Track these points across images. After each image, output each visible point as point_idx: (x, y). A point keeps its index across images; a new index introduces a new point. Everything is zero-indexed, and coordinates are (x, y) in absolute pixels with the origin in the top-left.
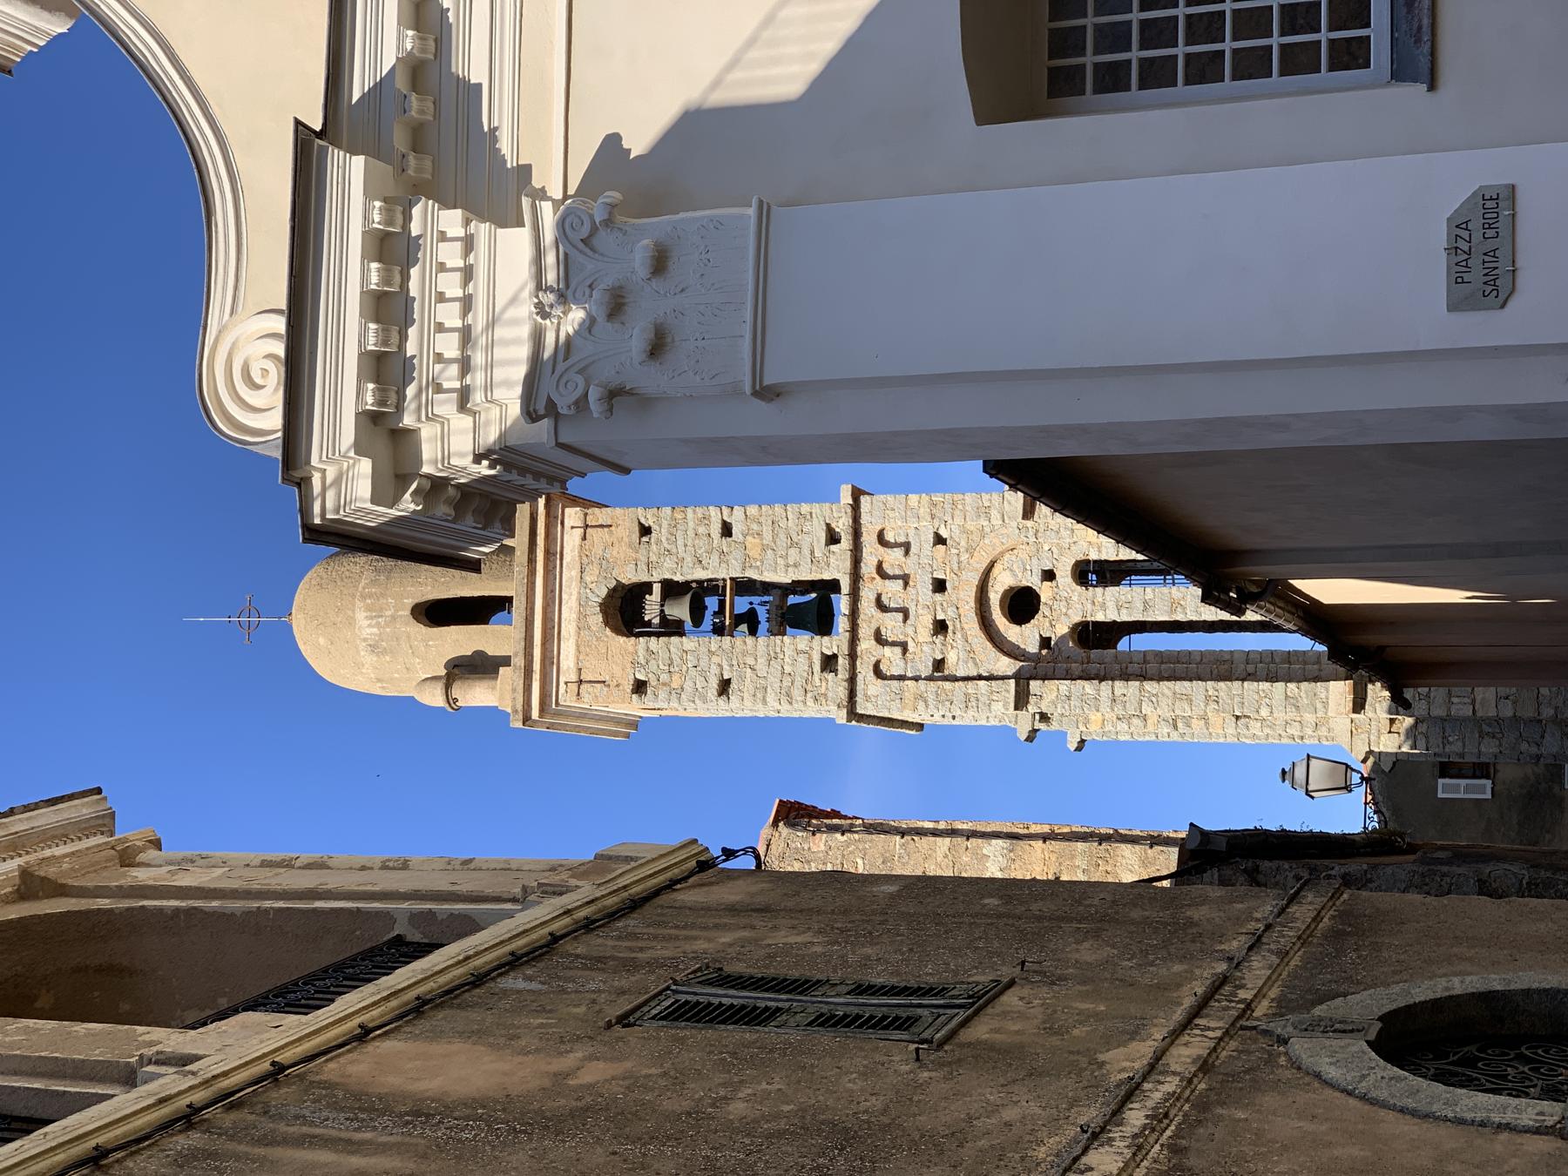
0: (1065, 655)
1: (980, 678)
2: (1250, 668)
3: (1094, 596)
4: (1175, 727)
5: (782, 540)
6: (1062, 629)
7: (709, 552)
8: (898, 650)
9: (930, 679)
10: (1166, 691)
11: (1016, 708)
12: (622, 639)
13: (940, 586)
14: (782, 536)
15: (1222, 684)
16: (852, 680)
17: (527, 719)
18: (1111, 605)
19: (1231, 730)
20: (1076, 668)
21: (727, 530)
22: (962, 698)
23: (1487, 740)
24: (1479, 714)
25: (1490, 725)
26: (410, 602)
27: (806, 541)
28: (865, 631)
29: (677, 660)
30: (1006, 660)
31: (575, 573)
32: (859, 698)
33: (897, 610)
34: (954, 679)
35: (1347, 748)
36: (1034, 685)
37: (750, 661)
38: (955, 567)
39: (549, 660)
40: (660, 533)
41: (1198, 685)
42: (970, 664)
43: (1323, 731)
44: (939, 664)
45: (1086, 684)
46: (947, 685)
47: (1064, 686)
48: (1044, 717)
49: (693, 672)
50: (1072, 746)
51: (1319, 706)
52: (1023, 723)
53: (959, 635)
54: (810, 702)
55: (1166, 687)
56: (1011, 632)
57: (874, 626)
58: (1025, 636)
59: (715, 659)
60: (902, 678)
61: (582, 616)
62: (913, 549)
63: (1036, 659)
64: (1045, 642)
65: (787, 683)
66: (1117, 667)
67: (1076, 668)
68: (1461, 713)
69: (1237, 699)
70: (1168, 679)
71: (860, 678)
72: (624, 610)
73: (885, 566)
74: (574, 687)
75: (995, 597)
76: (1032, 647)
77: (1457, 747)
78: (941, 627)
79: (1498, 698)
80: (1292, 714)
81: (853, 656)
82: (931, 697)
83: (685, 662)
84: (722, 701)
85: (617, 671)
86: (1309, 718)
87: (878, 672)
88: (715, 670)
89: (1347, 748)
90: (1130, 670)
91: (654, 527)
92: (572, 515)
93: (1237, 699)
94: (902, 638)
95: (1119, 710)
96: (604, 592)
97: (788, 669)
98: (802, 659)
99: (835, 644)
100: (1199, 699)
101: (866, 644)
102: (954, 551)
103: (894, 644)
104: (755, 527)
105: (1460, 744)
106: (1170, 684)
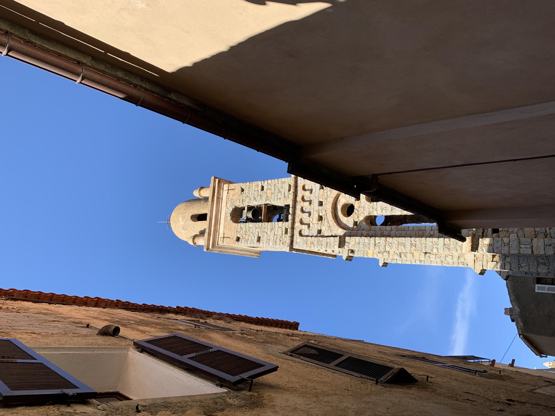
0: (362, 228)
1: (332, 236)
2: (432, 233)
3: (373, 205)
4: (401, 257)
5: (277, 191)
6: (361, 218)
7: (258, 196)
8: (306, 226)
9: (316, 236)
10: (395, 242)
11: (339, 247)
12: (234, 224)
13: (321, 204)
14: (277, 189)
15: (417, 239)
16: (292, 236)
17: (208, 249)
18: (379, 209)
19: (422, 258)
20: (365, 232)
21: (263, 188)
22: (325, 243)
23: (541, 266)
24: (535, 253)
25: (542, 259)
26: (190, 215)
27: (283, 190)
28: (297, 220)
29: (248, 231)
30: (341, 230)
31: (225, 204)
32: (294, 243)
33: (307, 212)
34: (323, 236)
35: (472, 267)
36: (347, 239)
37: (266, 230)
38: (326, 197)
39: (216, 230)
40: (246, 191)
41: (408, 239)
42: (329, 231)
43: (462, 260)
44: (320, 232)
45: (365, 238)
46: (321, 239)
47: (357, 239)
48: (352, 251)
49: (251, 234)
50: (381, 264)
51: (458, 248)
52: (344, 253)
53: (326, 221)
54: (281, 244)
55: (395, 240)
56: (345, 220)
57: (300, 218)
58: (349, 221)
59: (257, 230)
60: (308, 236)
61: (226, 217)
62: (313, 191)
63: (353, 229)
64: (355, 223)
65: (275, 237)
66: (380, 232)
67: (365, 232)
68: (525, 252)
69: (423, 245)
70: (396, 237)
71: (295, 236)
72: (237, 215)
73: (305, 197)
74: (222, 239)
75: (339, 207)
76: (351, 225)
77: (526, 269)
78: (321, 218)
79: (545, 246)
80: (447, 252)
81: (293, 228)
82: (315, 243)
83: (249, 231)
84: (258, 243)
85: (233, 234)
86: (456, 254)
87: (301, 234)
88: (257, 234)
89: (472, 267)
90: (384, 234)
91: (245, 189)
92: (226, 186)
93: (423, 245)
94: (309, 222)
95: (377, 249)
96: (231, 210)
97: (276, 233)
98: (280, 230)
99: (288, 225)
100: (408, 245)
101: (297, 224)
102: (326, 191)
103: (306, 224)
104: (270, 187)
105: (527, 267)
106: (397, 239)
